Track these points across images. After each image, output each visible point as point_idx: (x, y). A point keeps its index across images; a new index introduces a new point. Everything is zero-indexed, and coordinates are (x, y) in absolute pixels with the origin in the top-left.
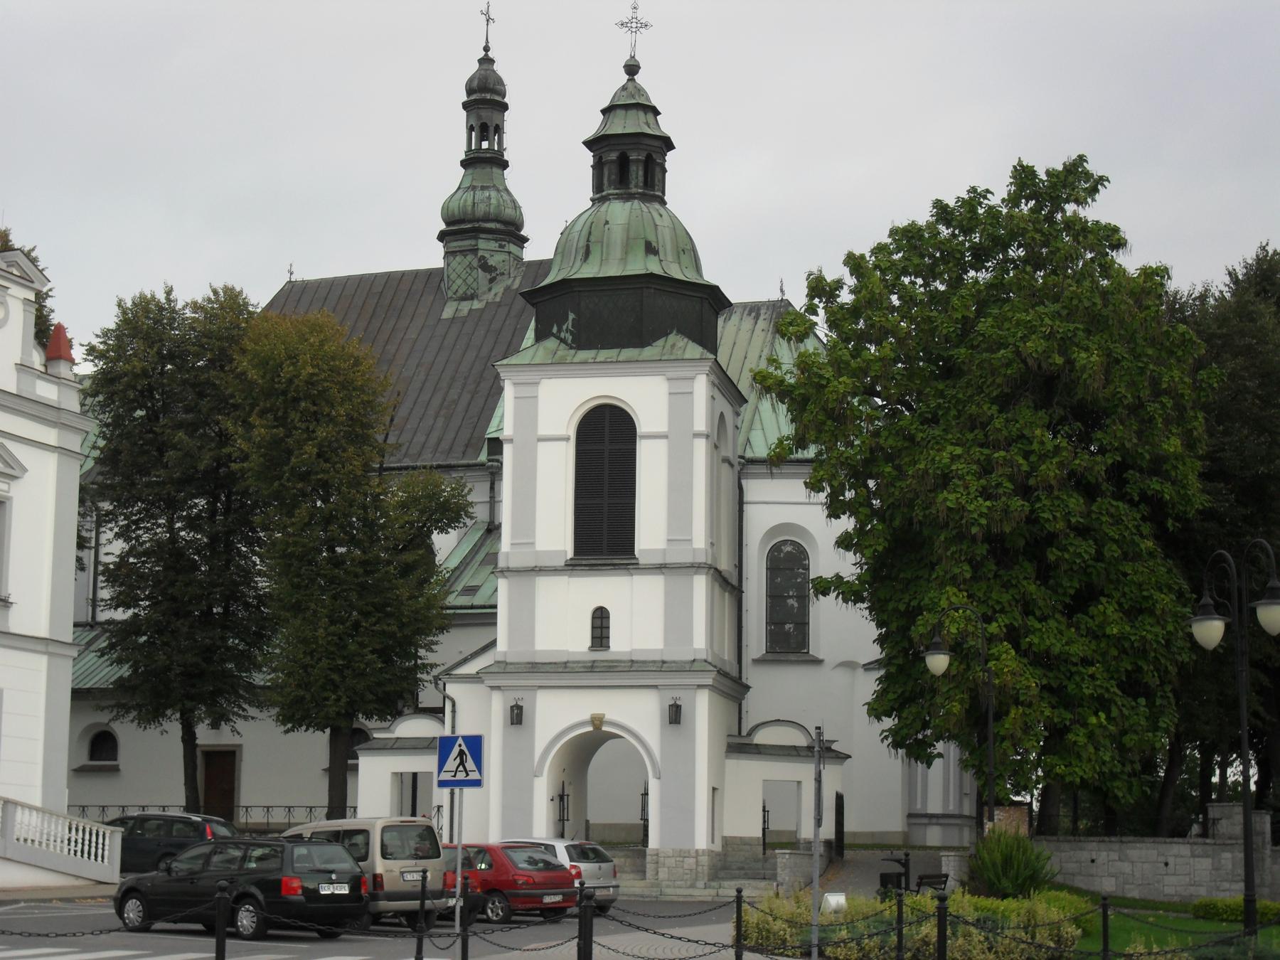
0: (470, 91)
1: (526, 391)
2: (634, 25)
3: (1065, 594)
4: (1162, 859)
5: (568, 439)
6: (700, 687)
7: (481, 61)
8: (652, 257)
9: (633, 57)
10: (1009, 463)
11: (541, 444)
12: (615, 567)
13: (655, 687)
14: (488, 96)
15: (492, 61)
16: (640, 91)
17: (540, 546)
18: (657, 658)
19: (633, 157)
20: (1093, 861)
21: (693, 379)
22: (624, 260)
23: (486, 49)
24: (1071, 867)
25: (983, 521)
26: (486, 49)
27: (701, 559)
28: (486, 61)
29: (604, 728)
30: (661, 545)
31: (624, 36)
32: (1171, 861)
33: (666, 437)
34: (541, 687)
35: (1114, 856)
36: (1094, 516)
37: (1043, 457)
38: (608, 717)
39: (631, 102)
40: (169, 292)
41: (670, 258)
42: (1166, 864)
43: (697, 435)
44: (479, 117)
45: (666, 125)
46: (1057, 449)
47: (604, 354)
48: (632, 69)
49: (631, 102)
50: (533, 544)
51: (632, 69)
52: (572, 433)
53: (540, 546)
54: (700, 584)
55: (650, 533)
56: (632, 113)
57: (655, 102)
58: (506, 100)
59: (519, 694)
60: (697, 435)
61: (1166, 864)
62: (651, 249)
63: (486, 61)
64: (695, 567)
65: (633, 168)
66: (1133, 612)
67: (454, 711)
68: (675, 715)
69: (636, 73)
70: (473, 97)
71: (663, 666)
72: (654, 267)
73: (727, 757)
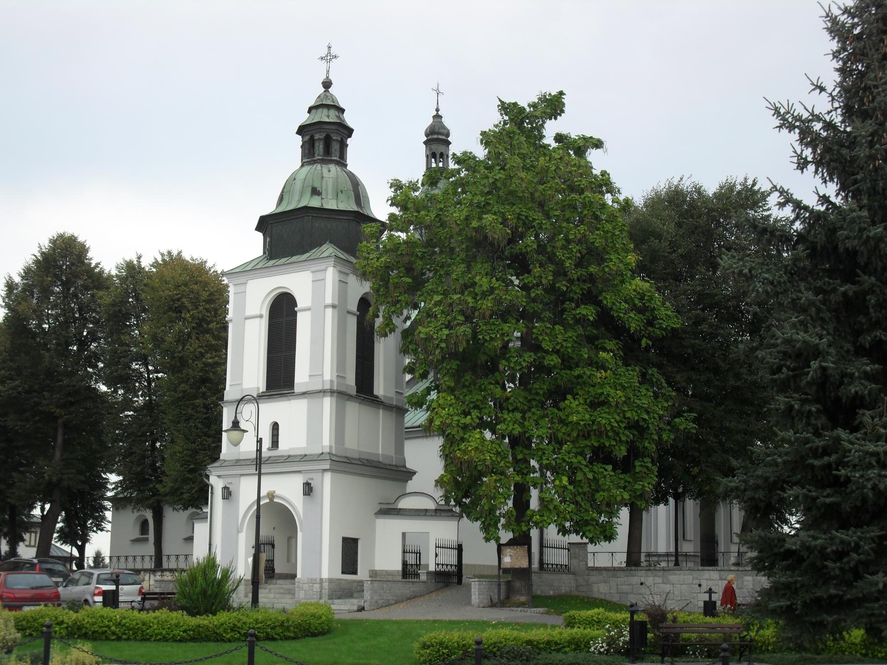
0: (427, 135)
1: (240, 289)
2: (329, 57)
3: (537, 394)
4: (697, 582)
5: (261, 316)
6: (325, 470)
7: (434, 117)
8: (316, 197)
9: (327, 77)
10: (462, 302)
11: (247, 321)
12: (282, 395)
13: (299, 472)
14: (435, 136)
15: (441, 117)
16: (333, 98)
17: (245, 386)
18: (303, 453)
19: (317, 137)
20: (642, 584)
21: (325, 270)
22: (299, 201)
23: (437, 110)
24: (625, 588)
25: (443, 345)
26: (437, 110)
27: (327, 387)
28: (437, 117)
29: (275, 500)
30: (307, 379)
31: (323, 65)
32: (704, 583)
33: (309, 309)
34: (242, 475)
35: (659, 580)
36: (534, 336)
37: (484, 295)
38: (277, 493)
39: (327, 104)
40: (139, 258)
41: (330, 197)
42: (700, 585)
43: (326, 307)
44: (431, 149)
45: (349, 119)
46: (492, 290)
47: (283, 260)
48: (327, 84)
49: (327, 104)
50: (241, 384)
51: (327, 84)
52: (265, 312)
53: (245, 386)
54: (327, 403)
55: (303, 374)
56: (320, 110)
57: (342, 105)
58: (449, 139)
59: (230, 480)
60: (326, 307)
61: (700, 585)
62: (315, 192)
63: (437, 117)
64: (323, 392)
65: (317, 144)
66: (596, 404)
67: (212, 493)
68: (308, 489)
69: (329, 87)
70: (430, 137)
71: (304, 458)
72: (315, 203)
73: (376, 517)
